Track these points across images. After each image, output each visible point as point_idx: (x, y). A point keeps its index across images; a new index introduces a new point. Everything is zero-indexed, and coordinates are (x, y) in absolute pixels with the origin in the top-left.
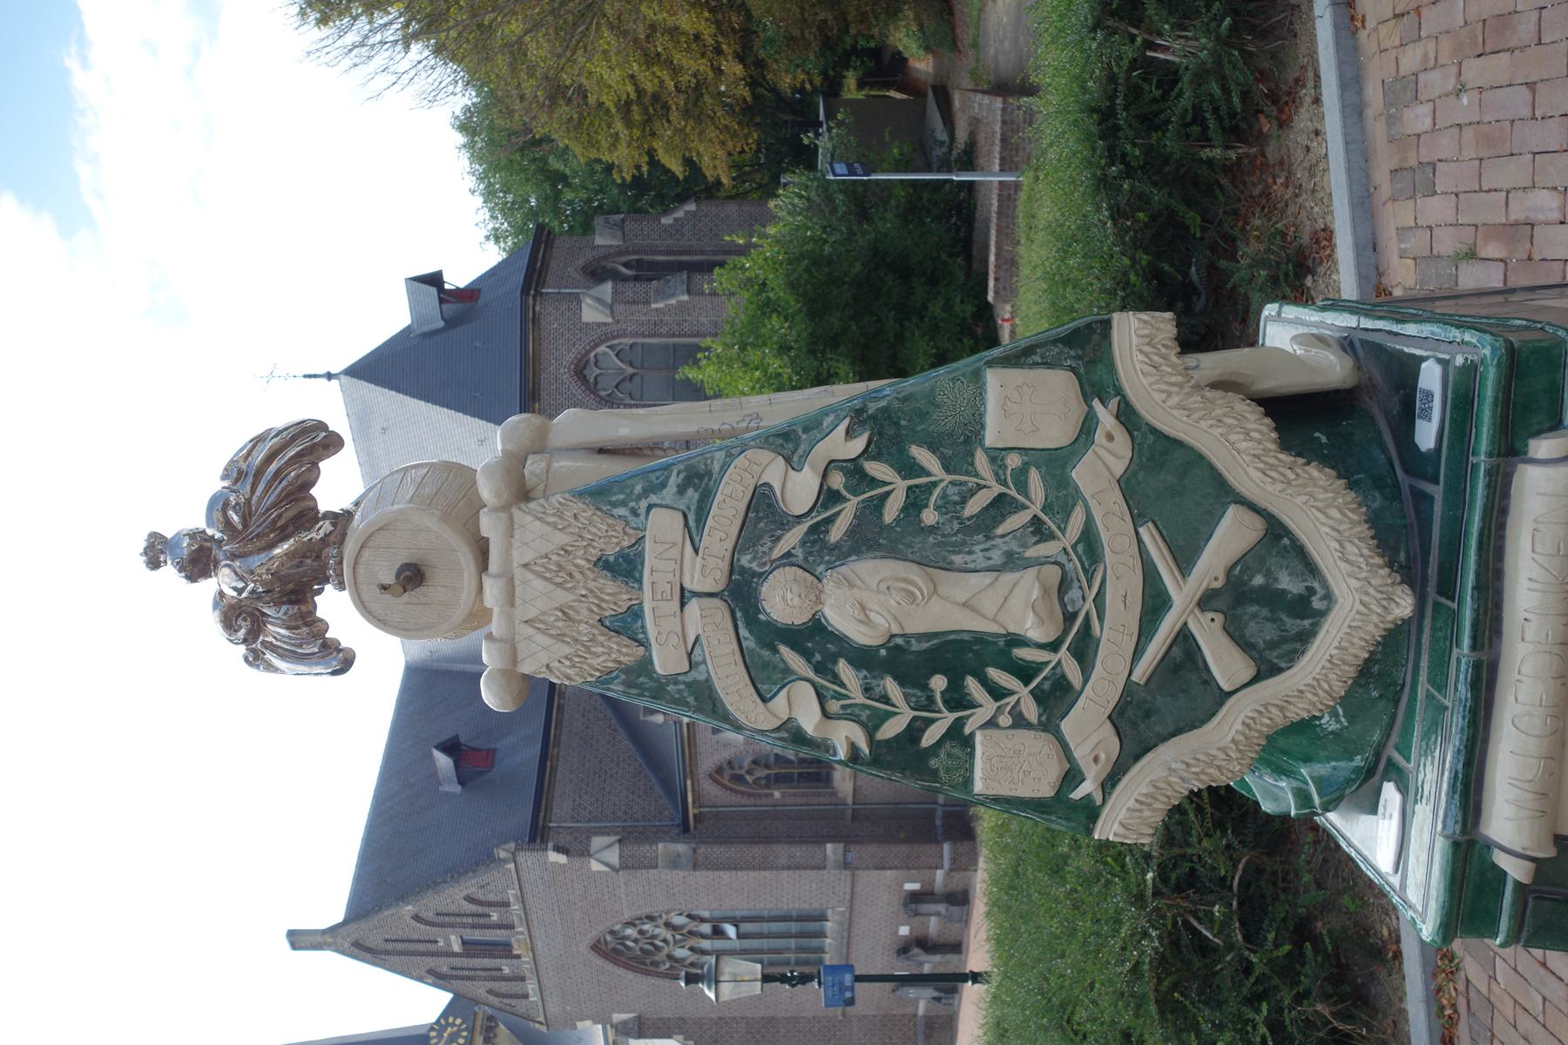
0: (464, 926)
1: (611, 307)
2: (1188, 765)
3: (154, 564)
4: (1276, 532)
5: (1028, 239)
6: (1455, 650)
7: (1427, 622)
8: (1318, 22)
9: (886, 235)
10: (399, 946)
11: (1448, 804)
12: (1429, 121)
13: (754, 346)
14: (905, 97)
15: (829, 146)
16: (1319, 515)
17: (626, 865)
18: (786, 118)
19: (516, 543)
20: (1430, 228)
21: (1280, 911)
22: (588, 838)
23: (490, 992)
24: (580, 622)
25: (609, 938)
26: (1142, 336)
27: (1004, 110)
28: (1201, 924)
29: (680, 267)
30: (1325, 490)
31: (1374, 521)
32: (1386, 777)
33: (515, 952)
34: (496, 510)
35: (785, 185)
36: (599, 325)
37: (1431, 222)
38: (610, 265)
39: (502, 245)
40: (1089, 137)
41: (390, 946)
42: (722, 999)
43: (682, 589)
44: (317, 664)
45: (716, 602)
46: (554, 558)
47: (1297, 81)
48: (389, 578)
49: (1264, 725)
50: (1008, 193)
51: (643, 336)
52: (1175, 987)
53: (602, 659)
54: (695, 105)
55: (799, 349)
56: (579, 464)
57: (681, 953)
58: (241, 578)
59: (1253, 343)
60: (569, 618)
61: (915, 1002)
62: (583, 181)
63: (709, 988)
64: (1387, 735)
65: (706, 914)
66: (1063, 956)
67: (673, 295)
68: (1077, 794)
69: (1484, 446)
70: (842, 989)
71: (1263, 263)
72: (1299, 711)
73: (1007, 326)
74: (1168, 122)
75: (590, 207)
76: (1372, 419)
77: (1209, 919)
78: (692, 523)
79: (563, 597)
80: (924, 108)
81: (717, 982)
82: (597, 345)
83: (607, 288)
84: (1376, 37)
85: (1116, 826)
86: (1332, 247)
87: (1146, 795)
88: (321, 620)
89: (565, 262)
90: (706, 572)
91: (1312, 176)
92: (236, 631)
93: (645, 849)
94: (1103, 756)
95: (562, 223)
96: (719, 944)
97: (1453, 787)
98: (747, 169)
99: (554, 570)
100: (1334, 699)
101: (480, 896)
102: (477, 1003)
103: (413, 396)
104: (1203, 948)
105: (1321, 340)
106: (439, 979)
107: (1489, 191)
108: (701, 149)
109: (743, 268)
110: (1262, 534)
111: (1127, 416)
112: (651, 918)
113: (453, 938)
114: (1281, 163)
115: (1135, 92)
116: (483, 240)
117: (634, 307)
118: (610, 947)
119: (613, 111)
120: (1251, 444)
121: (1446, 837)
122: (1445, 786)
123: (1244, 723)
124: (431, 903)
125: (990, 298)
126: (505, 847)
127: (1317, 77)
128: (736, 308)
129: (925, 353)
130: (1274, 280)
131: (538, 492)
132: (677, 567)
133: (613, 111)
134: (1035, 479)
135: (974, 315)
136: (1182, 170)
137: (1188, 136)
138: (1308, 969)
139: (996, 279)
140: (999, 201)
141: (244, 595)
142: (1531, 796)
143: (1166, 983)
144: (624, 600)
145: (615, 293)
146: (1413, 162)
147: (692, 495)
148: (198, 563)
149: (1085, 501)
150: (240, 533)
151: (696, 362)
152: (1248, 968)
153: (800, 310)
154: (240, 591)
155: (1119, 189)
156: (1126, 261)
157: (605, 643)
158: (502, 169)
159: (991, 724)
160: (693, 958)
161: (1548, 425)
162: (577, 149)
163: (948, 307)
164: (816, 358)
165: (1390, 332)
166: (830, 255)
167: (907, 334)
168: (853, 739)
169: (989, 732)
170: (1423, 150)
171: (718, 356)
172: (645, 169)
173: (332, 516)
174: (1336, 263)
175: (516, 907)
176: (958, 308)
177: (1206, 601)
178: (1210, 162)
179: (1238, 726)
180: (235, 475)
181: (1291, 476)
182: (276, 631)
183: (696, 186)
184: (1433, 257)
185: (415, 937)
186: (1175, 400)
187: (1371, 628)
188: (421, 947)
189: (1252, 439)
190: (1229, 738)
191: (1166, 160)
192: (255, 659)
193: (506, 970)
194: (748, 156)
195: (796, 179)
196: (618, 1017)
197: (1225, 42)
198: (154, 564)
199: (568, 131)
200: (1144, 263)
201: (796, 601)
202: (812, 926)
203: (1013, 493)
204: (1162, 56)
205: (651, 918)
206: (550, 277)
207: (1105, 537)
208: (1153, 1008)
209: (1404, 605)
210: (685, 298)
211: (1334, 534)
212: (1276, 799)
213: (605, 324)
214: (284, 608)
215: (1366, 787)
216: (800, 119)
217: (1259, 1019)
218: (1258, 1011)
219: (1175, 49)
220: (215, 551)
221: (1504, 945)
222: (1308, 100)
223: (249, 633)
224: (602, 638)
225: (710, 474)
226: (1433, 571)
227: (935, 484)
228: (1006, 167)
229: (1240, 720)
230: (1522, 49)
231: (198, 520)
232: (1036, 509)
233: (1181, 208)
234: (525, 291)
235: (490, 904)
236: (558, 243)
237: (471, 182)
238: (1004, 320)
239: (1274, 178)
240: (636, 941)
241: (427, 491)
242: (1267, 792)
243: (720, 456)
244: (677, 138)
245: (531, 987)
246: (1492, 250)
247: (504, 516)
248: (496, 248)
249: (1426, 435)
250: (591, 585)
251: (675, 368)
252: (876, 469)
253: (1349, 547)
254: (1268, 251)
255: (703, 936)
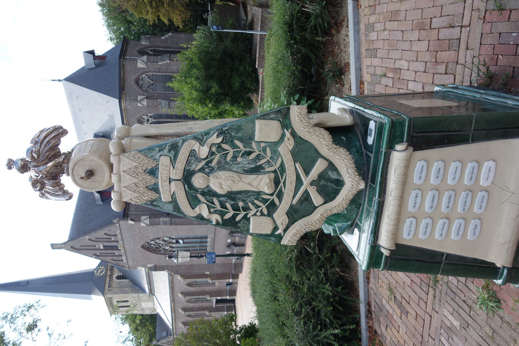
0: (104, 242)
1: (146, 63)
2: (306, 225)
3: (10, 168)
4: (331, 166)
5: (268, 51)
6: (374, 198)
7: (368, 191)
8: (349, 5)
9: (228, 47)
10: (85, 248)
11: (370, 236)
12: (376, 37)
13: (189, 77)
14: (234, 5)
15: (211, 19)
16: (342, 161)
17: (151, 224)
18: (199, 8)
19: (121, 165)
20: (375, 66)
21: (328, 244)
22: (140, 217)
23: (112, 260)
24: (140, 187)
25: (146, 244)
26: (298, 112)
27: (262, 12)
28: (308, 247)
29: (167, 52)
30: (344, 155)
31: (356, 163)
32: (355, 227)
33: (119, 249)
34: (115, 155)
35: (199, 29)
36: (143, 68)
37: (375, 65)
38: (146, 50)
39: (113, 42)
40: (285, 32)
41: (82, 248)
42: (179, 262)
43: (170, 179)
44: (62, 197)
45: (179, 182)
46: (133, 169)
47: (342, 20)
48: (83, 175)
49: (326, 215)
50: (262, 37)
51: (156, 72)
52: (300, 264)
53: (147, 197)
54: (172, 3)
55: (202, 79)
56: (139, 141)
57: (167, 248)
58: (38, 173)
59: (328, 111)
60: (137, 186)
61: (232, 260)
62: (137, 24)
63: (175, 259)
64: (356, 216)
65: (174, 237)
66: (272, 254)
67: (165, 61)
68: (277, 233)
69: (384, 147)
70: (212, 259)
71: (331, 71)
72: (335, 211)
73: (261, 75)
74: (307, 29)
75: (140, 32)
76: (357, 133)
77: (310, 247)
78: (173, 161)
79: (135, 180)
80: (239, 8)
81: (177, 258)
82: (142, 74)
83: (145, 58)
84: (364, 11)
85: (287, 241)
86: (349, 68)
87: (295, 233)
88: (62, 184)
89: (132, 48)
90: (177, 173)
91: (345, 47)
92: (36, 188)
93: (157, 220)
94: (284, 223)
95: (131, 36)
96: (178, 245)
97: (372, 232)
98: (187, 23)
99: (133, 172)
100: (344, 209)
101: (109, 233)
102: (108, 262)
103: (86, 87)
104: (308, 254)
105: (344, 109)
106: (97, 256)
107: (390, 59)
108: (173, 16)
109: (185, 54)
110: (327, 166)
111: (294, 134)
112: (158, 239)
113: (101, 245)
114: (337, 43)
115: (298, 19)
116: (107, 40)
117: (153, 63)
118: (147, 246)
119: (147, 3)
120: (325, 142)
121: (369, 244)
122: (370, 232)
123: (321, 215)
124: (94, 235)
125: (257, 67)
126: (116, 219)
127: (348, 20)
128: (183, 66)
129: (238, 82)
130: (334, 76)
131: (127, 150)
132: (168, 173)
133: (147, 3)
134: (268, 150)
135: (252, 71)
136: (310, 43)
137: (312, 33)
138: (334, 259)
139: (258, 61)
140: (260, 39)
141: (39, 178)
142: (391, 235)
143: (298, 263)
144: (153, 181)
145: (147, 59)
146: (371, 48)
147: (173, 152)
148: (24, 168)
149: (281, 156)
150: (37, 160)
151: (172, 81)
152: (319, 259)
153: (202, 67)
154: (37, 177)
155: (293, 48)
156: (295, 68)
157: (148, 193)
158: (113, 19)
159: (255, 215)
160: (170, 249)
161: (400, 141)
162: (136, 14)
163: (245, 68)
164: (207, 82)
165: (362, 111)
166: (211, 51)
167: (233, 76)
168: (217, 219)
169: (254, 217)
170: (374, 45)
171: (178, 80)
172: (157, 21)
173: (64, 154)
174: (350, 72)
175: (119, 236)
176: (247, 69)
177: (312, 183)
178: (318, 41)
179: (319, 215)
180: (34, 142)
181: (335, 151)
182: (48, 187)
183: (172, 28)
184: (375, 75)
185: (89, 245)
186: (306, 130)
187: (354, 191)
188: (91, 248)
189: (326, 141)
190: (317, 218)
191: (306, 40)
192: (43, 195)
193: (117, 254)
194: (188, 19)
195: (201, 28)
196: (149, 266)
197: (324, 8)
198: (10, 168)
199: (133, 9)
200: (299, 69)
201: (202, 182)
202: (204, 240)
203: (262, 153)
204: (306, 10)
205: (158, 239)
206: (128, 53)
207: (286, 166)
208: (294, 269)
209: (362, 186)
210: (169, 61)
211: (346, 166)
212: (328, 230)
213: (145, 68)
214: (51, 181)
215: (350, 229)
216: (203, 9)
217: (321, 272)
218: (322, 271)
219: (309, 8)
220: (29, 164)
221: (382, 270)
222: (345, 26)
223: (40, 188)
224: (146, 192)
225: (178, 147)
226: (370, 176)
227: (241, 151)
228: (262, 29)
229: (320, 214)
230: (401, 21)
231: (23, 155)
232: (268, 158)
233: (310, 54)
234: (120, 57)
235: (112, 235)
236: (130, 43)
237: (103, 22)
238: (260, 73)
239: (335, 47)
240: (154, 245)
241: (94, 148)
242: (326, 229)
243: (181, 141)
244: (166, 12)
245: (124, 258)
246: (390, 75)
247: (117, 157)
248: (111, 43)
249: (370, 140)
250: (143, 177)
251: (165, 82)
252: (225, 146)
253: (349, 170)
254: (332, 67)
255: (173, 243)
